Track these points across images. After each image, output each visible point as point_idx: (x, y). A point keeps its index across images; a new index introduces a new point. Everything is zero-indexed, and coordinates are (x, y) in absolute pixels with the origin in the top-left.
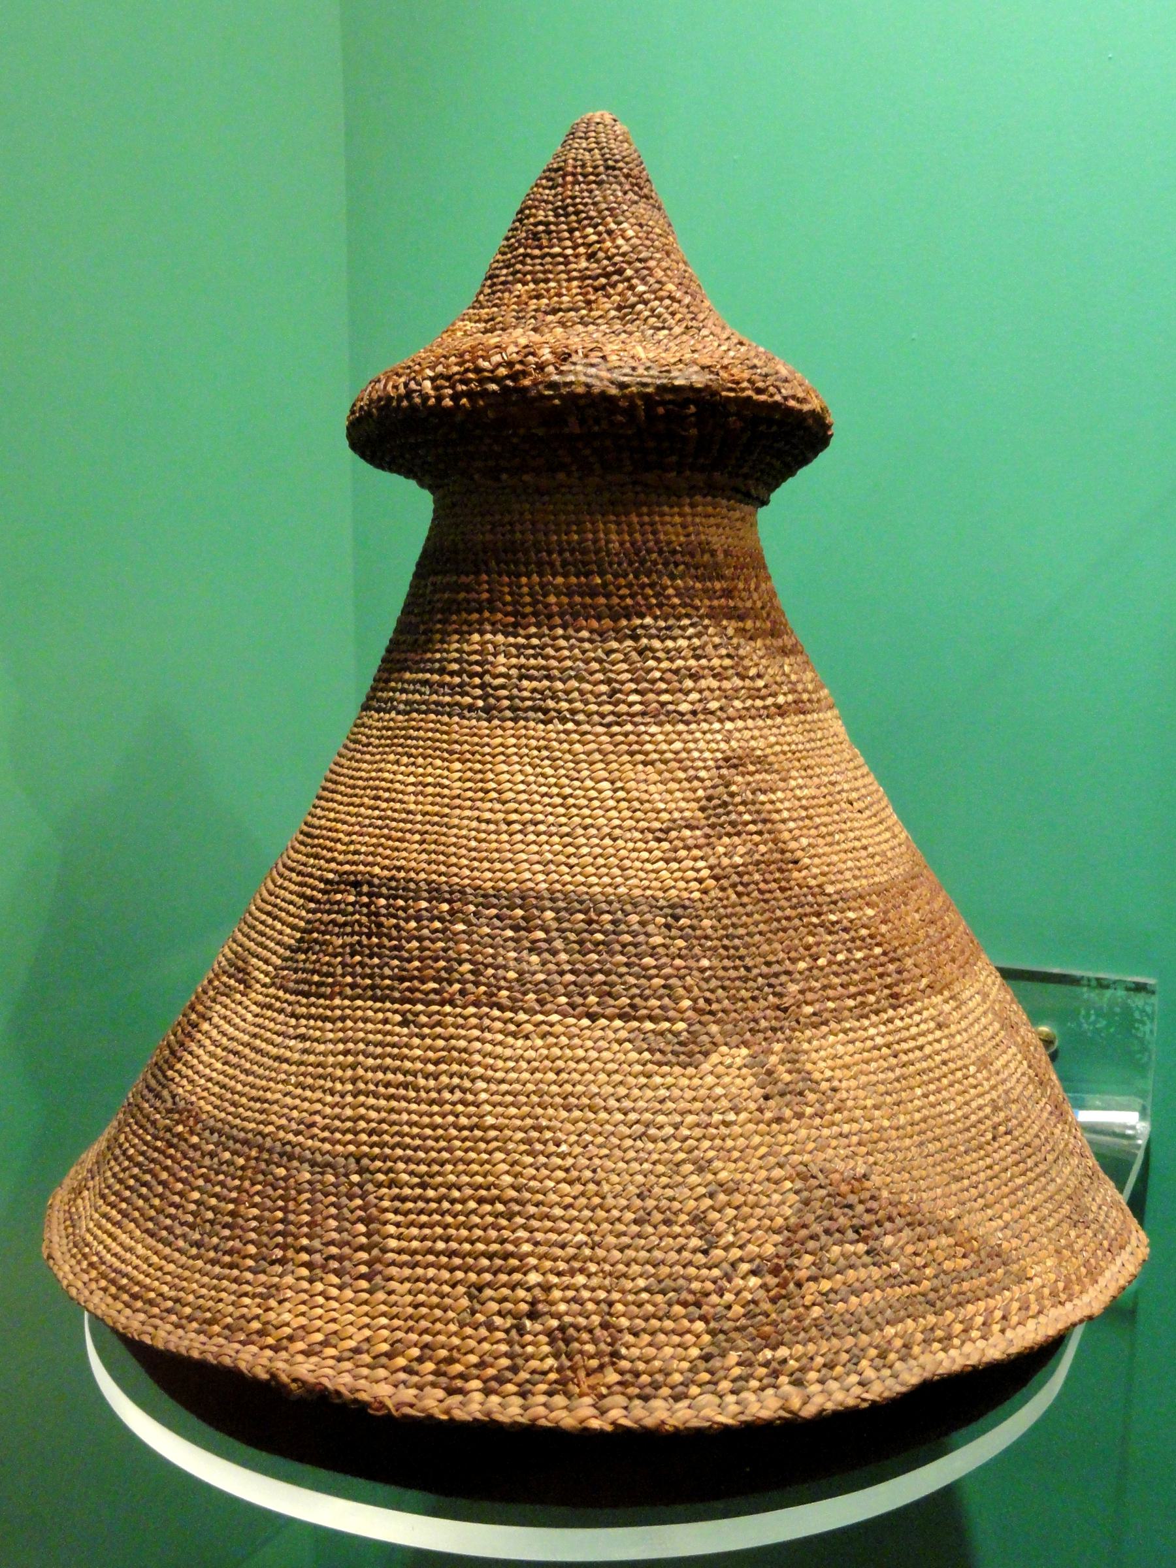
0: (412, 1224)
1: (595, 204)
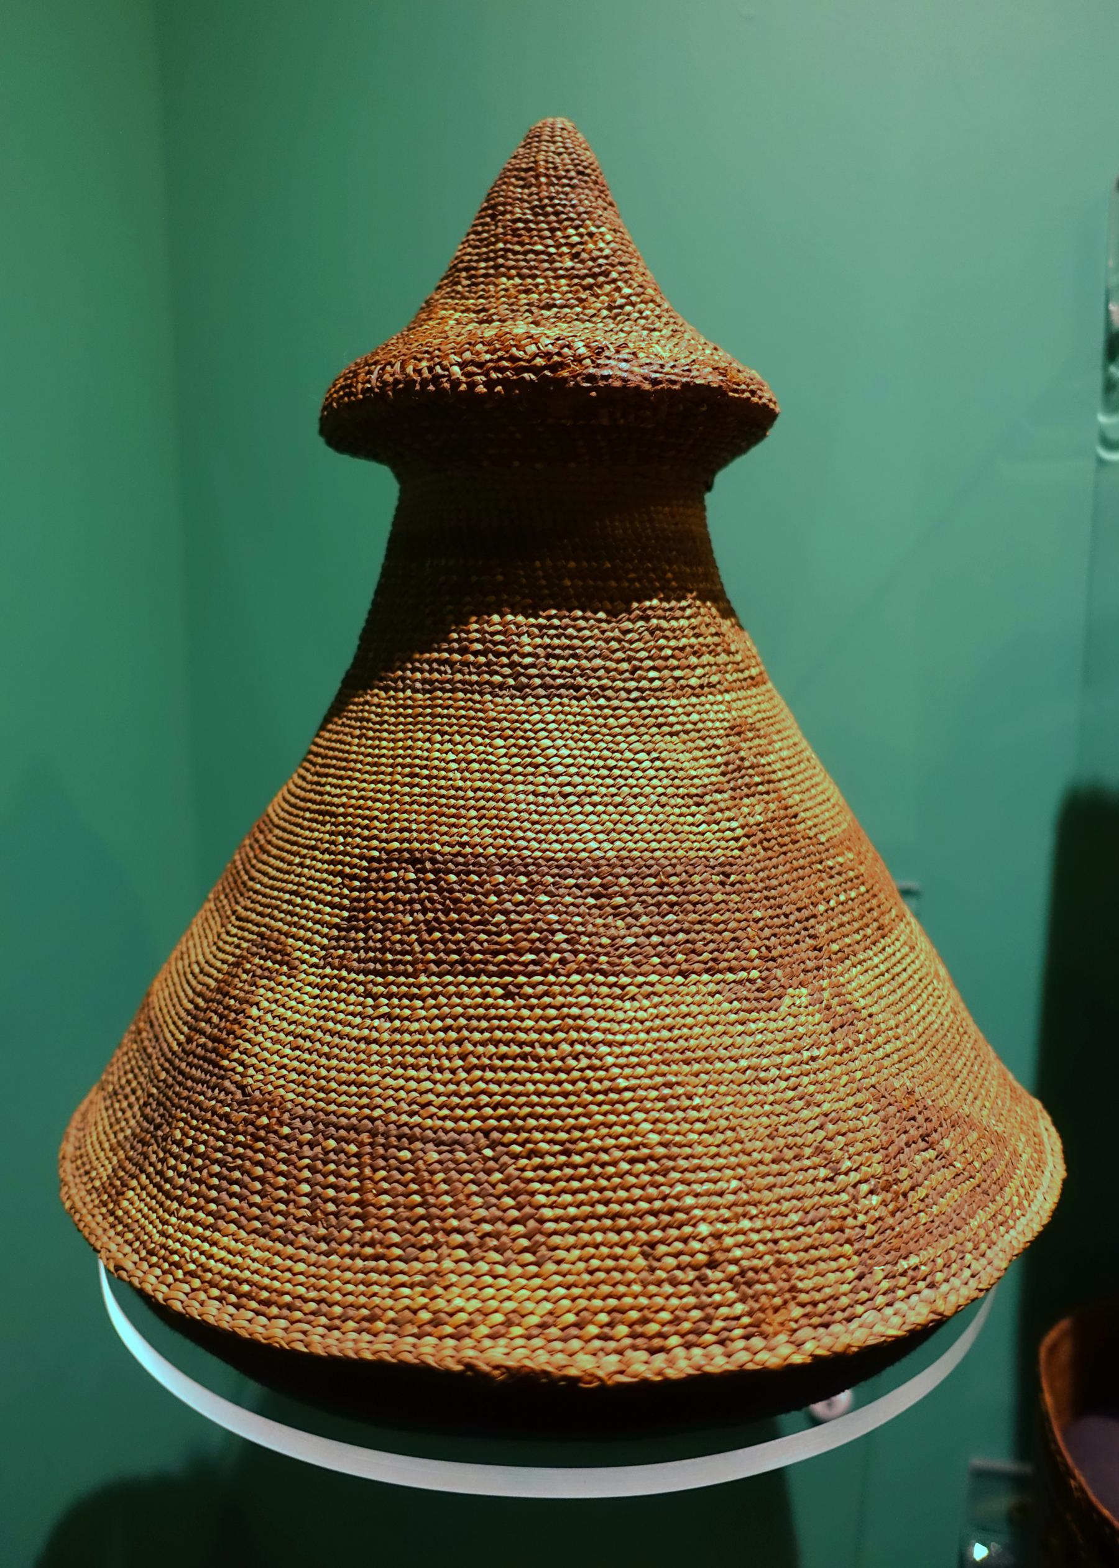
0: (563, 1191)
1: (573, 206)
